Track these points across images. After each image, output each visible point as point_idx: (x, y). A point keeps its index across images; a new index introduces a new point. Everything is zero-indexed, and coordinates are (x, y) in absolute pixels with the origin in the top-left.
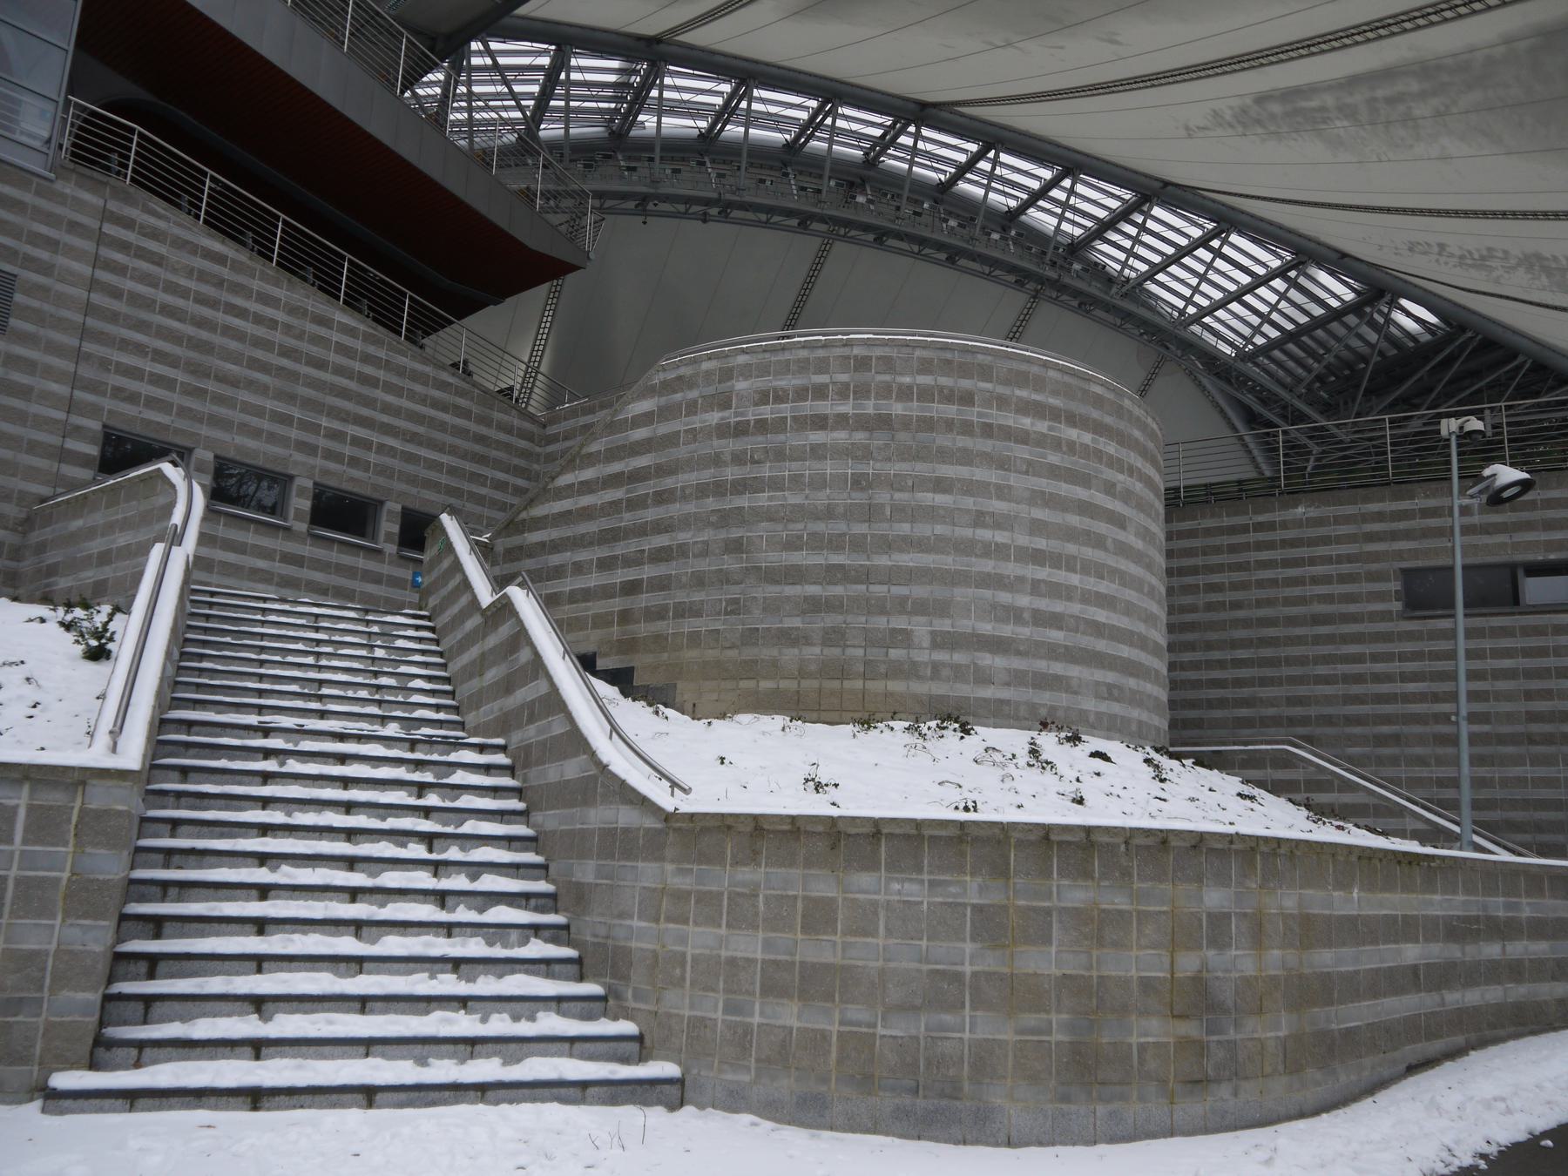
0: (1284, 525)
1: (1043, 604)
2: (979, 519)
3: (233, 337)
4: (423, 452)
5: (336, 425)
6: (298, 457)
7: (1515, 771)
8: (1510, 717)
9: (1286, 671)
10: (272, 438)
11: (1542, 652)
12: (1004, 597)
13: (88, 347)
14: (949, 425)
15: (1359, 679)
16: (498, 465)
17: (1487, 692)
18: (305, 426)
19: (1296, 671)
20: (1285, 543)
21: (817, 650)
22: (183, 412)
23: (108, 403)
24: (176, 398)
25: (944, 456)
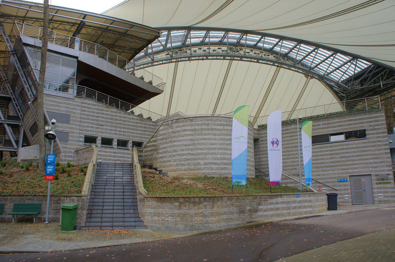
0: (290, 129)
1: (222, 156)
2: (211, 144)
3: (102, 118)
4: (135, 131)
5: (120, 129)
6: (115, 136)
7: (329, 172)
8: (328, 163)
9: (291, 156)
10: (110, 133)
11: (333, 150)
12: (216, 156)
13: (81, 124)
14: (205, 129)
15: (347, 149)
16: (148, 131)
17: (324, 158)
18: (115, 130)
19: (293, 156)
20: (291, 133)
21: (186, 166)
22: (96, 131)
23: (85, 132)
24: (95, 130)
25: (205, 134)
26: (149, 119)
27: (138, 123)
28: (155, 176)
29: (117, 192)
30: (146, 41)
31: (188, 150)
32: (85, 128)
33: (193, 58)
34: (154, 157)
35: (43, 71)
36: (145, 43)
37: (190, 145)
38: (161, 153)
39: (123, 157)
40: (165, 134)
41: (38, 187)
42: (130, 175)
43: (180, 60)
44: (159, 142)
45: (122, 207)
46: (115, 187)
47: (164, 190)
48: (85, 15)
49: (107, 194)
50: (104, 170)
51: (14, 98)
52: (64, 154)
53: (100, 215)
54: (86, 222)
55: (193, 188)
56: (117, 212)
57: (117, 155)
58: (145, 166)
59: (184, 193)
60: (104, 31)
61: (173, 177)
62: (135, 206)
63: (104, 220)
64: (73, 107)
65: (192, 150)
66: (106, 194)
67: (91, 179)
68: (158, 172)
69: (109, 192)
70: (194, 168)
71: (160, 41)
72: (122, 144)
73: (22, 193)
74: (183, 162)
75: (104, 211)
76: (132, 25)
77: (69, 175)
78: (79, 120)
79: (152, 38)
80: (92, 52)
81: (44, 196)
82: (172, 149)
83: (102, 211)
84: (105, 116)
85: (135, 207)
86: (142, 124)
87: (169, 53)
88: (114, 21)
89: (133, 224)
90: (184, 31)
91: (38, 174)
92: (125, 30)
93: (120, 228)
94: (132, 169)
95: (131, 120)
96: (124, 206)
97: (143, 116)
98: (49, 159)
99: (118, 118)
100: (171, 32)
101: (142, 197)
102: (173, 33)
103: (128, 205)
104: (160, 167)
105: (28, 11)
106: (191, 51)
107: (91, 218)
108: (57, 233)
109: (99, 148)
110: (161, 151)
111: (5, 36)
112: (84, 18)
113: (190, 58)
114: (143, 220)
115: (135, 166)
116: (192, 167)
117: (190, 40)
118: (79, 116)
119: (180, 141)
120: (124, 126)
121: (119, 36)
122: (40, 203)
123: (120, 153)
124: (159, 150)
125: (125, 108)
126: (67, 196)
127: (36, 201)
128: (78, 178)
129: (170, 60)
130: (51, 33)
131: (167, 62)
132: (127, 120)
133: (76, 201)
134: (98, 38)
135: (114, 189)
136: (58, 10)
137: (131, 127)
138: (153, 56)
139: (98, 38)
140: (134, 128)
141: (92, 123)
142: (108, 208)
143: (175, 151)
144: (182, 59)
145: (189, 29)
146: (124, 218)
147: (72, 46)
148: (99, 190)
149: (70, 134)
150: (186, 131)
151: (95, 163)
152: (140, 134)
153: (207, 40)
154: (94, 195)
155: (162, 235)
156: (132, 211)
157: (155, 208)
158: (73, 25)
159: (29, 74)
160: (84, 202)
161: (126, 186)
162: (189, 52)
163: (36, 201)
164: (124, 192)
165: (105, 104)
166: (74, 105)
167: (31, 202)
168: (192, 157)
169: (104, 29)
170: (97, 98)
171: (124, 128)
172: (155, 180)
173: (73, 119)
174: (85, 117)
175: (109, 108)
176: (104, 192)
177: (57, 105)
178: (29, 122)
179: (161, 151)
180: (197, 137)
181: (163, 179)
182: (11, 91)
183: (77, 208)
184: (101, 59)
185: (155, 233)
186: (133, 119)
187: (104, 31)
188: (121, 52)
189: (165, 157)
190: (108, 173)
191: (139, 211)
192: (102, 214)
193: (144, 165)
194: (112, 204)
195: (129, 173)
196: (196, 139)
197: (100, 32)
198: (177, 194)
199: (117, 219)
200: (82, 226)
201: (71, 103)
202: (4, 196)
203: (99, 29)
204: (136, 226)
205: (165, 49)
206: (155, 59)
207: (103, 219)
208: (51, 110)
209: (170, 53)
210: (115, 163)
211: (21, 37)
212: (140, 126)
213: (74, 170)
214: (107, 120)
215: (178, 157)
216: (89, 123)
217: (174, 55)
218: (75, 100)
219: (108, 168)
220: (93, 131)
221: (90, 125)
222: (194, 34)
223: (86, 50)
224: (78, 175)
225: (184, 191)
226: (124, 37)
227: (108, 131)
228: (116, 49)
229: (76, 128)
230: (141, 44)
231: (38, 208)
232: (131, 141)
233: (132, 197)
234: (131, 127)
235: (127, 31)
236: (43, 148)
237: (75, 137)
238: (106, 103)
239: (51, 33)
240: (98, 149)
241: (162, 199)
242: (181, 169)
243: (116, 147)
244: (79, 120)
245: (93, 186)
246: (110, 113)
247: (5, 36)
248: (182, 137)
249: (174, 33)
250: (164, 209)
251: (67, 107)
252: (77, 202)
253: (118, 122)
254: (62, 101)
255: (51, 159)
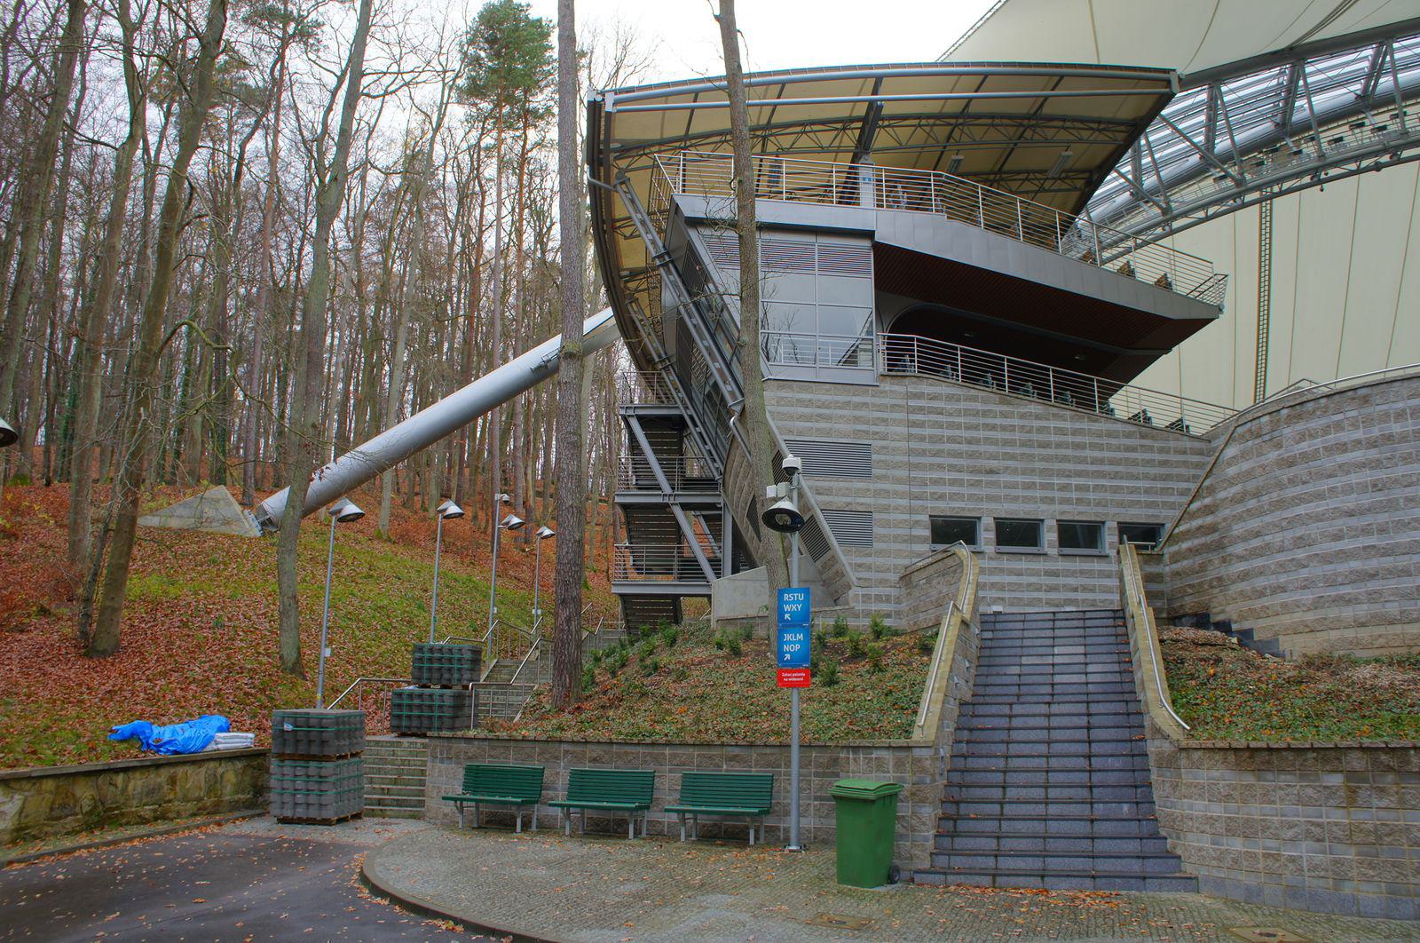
4: (1125, 483)
5: (1064, 481)
6: (1044, 507)
10: (1026, 499)
13: (913, 474)
16: (1180, 478)
21: (1365, 607)
22: (971, 497)
23: (929, 504)
24: (965, 491)
26: (1178, 427)
27: (1134, 449)
28: (1222, 654)
29: (1060, 728)
30: (1123, 128)
31: (1366, 531)
32: (930, 489)
33: (1333, 172)
34: (1212, 573)
35: (750, 294)
36: (1121, 136)
37: (1369, 510)
38: (1241, 558)
39: (1085, 589)
40: (1248, 475)
41: (764, 713)
42: (1115, 658)
43: (1276, 189)
44: (1227, 512)
45: (1084, 793)
46: (1055, 709)
47: (1269, 716)
48: (877, 78)
49: (1019, 738)
50: (1009, 643)
51: (691, 418)
52: (860, 592)
53: (991, 826)
54: (936, 854)
55: (1412, 706)
56: (1065, 813)
57: (1061, 581)
58: (1176, 618)
59: (1364, 728)
60: (956, 125)
61: (1305, 655)
62: (1139, 792)
63: (1007, 844)
64: (879, 414)
65: (1382, 530)
66: (1015, 735)
67: (950, 678)
68: (1235, 640)
69: (1029, 729)
70: (1402, 612)
71: (1185, 132)
72: (1078, 536)
73: (711, 736)
74: (1346, 590)
75: (1009, 810)
76: (1057, 74)
77: (877, 667)
78: (905, 459)
79: (1143, 112)
80: (919, 204)
81: (781, 746)
82: (1289, 535)
83: (1002, 808)
84: (999, 435)
85: (1139, 790)
86: (1150, 449)
87: (1229, 170)
88: (986, 75)
89: (1136, 866)
90: (1276, 71)
91: (770, 666)
92: (1033, 99)
93: (1074, 881)
94: (1121, 630)
95: (1105, 440)
96: (1091, 787)
97: (1149, 419)
98: (787, 608)
99: (1053, 438)
100: (1224, 89)
101: (1166, 747)
102: (1232, 91)
103: (1110, 783)
104: (1242, 617)
105: (692, 110)
106: (1319, 144)
107: (954, 834)
108: (819, 895)
109: (991, 558)
110: (1239, 549)
111: (637, 210)
112: (875, 92)
113: (1317, 175)
114: (1179, 852)
115: (1133, 617)
116: (1393, 609)
117: (1310, 102)
118: (904, 445)
119: (1319, 496)
120: (1081, 467)
121: (1017, 130)
122: (767, 772)
123: (1075, 572)
124: (1232, 544)
125: (1076, 397)
126: (856, 749)
127: (756, 765)
128: (912, 676)
129: (1233, 197)
130: (775, 172)
131: (1224, 208)
132: (1087, 440)
133: (891, 767)
134: (942, 152)
135: (1048, 716)
136: (781, 83)
137: (1106, 468)
138: (1167, 197)
139: (942, 152)
140: (1120, 468)
141: (952, 468)
142: (1023, 793)
143: (1300, 542)
144: (1286, 186)
145: (1296, 55)
146: (1093, 839)
147: (849, 196)
148: (989, 723)
149: (875, 516)
150: (1345, 451)
151: (967, 616)
152: (1147, 491)
153: (1385, 82)
154: (968, 742)
155: (1270, 930)
156: (1126, 807)
157: (1228, 797)
158: (844, 129)
159: (717, 323)
160: (924, 770)
161: (1098, 702)
162: (1309, 149)
163: (756, 765)
164: (1089, 728)
165: (995, 390)
166: (880, 408)
167: (737, 769)
168: (1388, 562)
169: (956, 117)
170: (962, 372)
171: (1079, 474)
172: (1224, 672)
173: (883, 458)
174: (926, 446)
175: (1009, 403)
176: (1009, 729)
177: (819, 415)
178: (741, 490)
179: (1239, 549)
180: (1400, 471)
181: (1258, 668)
182: (682, 395)
183: (893, 796)
184: (957, 224)
185: (1236, 914)
186: (1110, 434)
187: (956, 125)
188: (1031, 192)
189: (1261, 572)
190: (1026, 651)
191: (1160, 809)
192: (1000, 820)
193: (1173, 614)
194: (1040, 778)
195: (1113, 648)
196: (1396, 481)
197: (941, 132)
198: (1328, 732)
199: (1062, 845)
200: (920, 867)
201: (868, 399)
202: (653, 744)
203: (938, 122)
204: (1144, 878)
205: (1209, 161)
206: (1173, 205)
207: (1003, 841)
208: (800, 434)
209: (1233, 171)
210: (1054, 613)
211: (678, 200)
212: (1143, 460)
213: (894, 646)
214: (1008, 450)
215: (1318, 570)
216: (940, 467)
217: (1248, 177)
218: (881, 388)
219: (1026, 634)
220: (960, 497)
221: (948, 476)
222: (1320, 71)
223: (899, 202)
224: (910, 663)
225: (1364, 717)
226: (1034, 132)
227: (1020, 492)
228: (1014, 185)
229: (896, 493)
230: (1103, 142)
231: (764, 791)
232: (1111, 525)
233: (1125, 748)
234: (1106, 468)
235: (1041, 106)
236: (780, 572)
237: (897, 525)
238: (998, 385)
239: (775, 172)
240: (986, 564)
241: (1259, 758)
242: (1339, 620)
243: (1053, 551)
244: (905, 459)
245: (963, 704)
246: (1016, 422)
247: (637, 210)
248: (1330, 476)
249: (1233, 91)
250: (1273, 802)
251: (857, 419)
252: (894, 772)
253: (1052, 451)
254: (836, 398)
255: (794, 607)
